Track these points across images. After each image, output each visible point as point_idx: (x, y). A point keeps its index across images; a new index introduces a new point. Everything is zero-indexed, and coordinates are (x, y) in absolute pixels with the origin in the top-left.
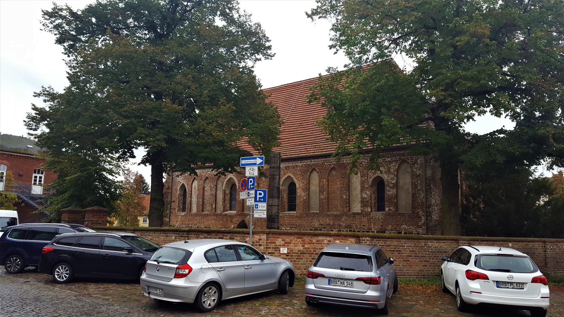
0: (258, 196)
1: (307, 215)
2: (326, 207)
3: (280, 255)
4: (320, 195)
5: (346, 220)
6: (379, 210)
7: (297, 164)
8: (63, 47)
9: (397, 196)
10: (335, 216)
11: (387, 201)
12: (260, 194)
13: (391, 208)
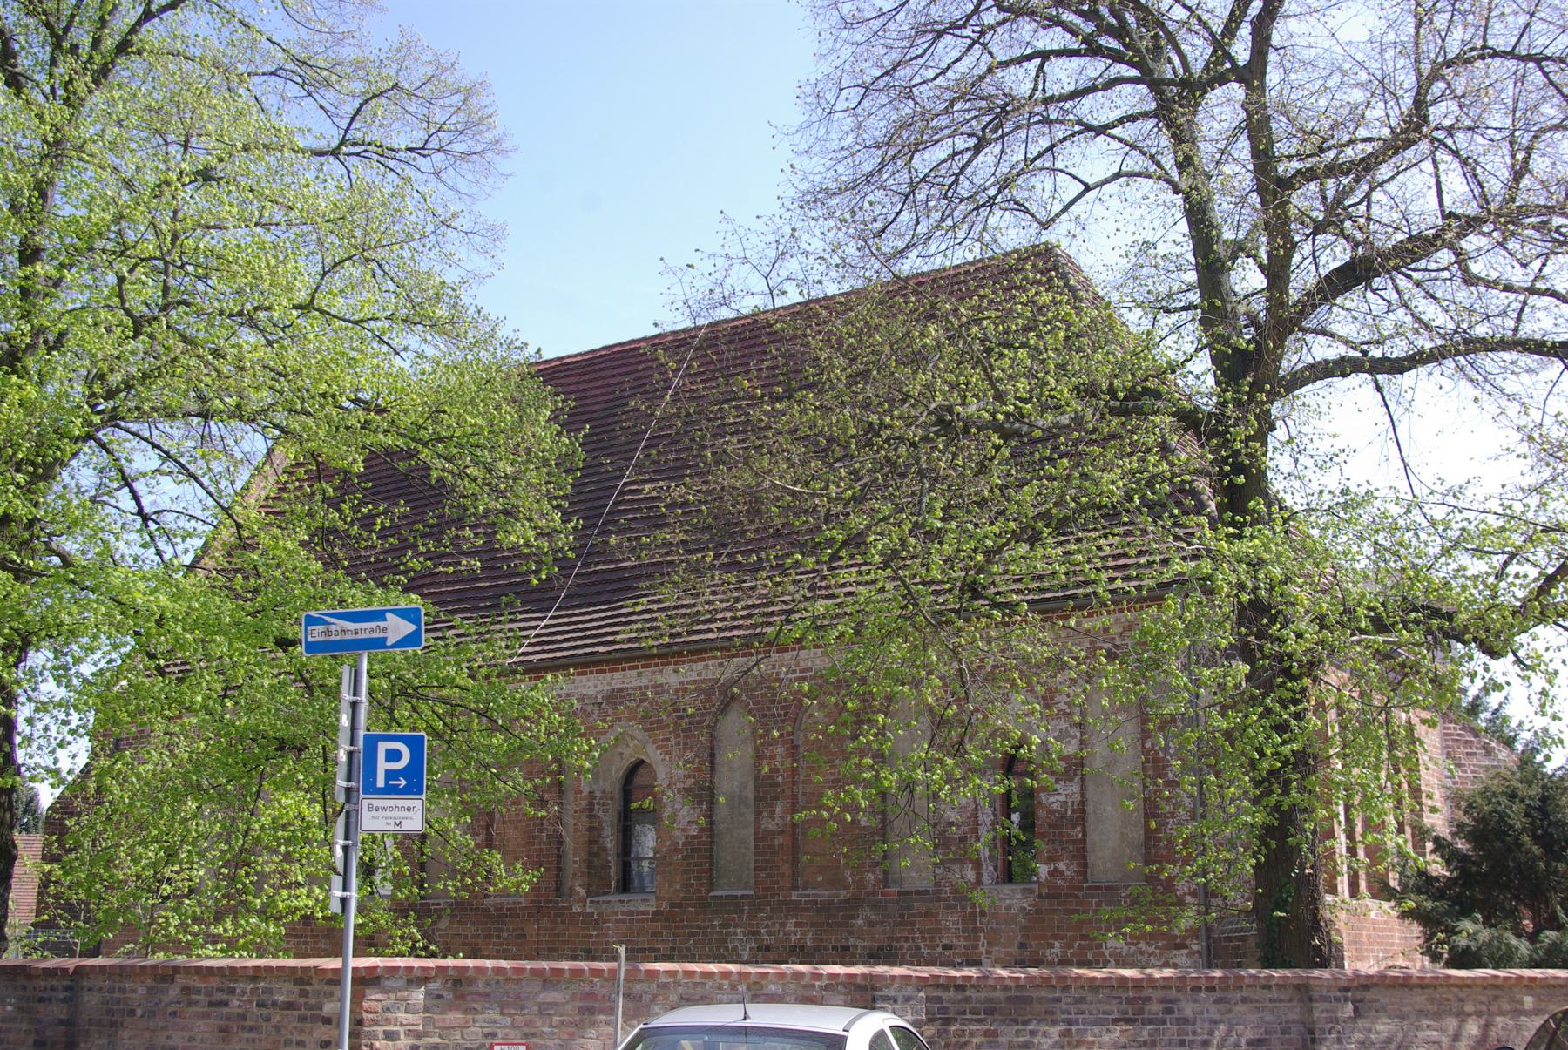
0: (383, 766)
1: (704, 905)
2: (786, 868)
3: (327, 897)
4: (758, 814)
5: (870, 924)
6: (1008, 876)
7: (660, 679)
8: (1115, 144)
9: (1081, 814)
10: (826, 908)
11: (1042, 836)
12: (393, 756)
13: (1062, 866)
